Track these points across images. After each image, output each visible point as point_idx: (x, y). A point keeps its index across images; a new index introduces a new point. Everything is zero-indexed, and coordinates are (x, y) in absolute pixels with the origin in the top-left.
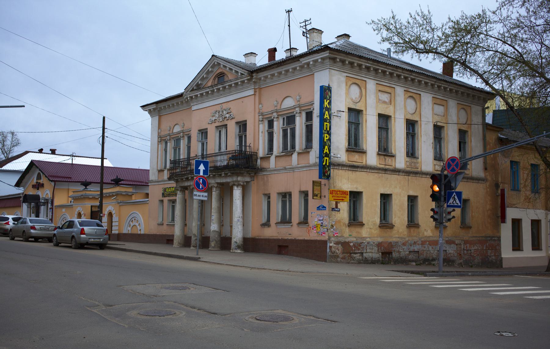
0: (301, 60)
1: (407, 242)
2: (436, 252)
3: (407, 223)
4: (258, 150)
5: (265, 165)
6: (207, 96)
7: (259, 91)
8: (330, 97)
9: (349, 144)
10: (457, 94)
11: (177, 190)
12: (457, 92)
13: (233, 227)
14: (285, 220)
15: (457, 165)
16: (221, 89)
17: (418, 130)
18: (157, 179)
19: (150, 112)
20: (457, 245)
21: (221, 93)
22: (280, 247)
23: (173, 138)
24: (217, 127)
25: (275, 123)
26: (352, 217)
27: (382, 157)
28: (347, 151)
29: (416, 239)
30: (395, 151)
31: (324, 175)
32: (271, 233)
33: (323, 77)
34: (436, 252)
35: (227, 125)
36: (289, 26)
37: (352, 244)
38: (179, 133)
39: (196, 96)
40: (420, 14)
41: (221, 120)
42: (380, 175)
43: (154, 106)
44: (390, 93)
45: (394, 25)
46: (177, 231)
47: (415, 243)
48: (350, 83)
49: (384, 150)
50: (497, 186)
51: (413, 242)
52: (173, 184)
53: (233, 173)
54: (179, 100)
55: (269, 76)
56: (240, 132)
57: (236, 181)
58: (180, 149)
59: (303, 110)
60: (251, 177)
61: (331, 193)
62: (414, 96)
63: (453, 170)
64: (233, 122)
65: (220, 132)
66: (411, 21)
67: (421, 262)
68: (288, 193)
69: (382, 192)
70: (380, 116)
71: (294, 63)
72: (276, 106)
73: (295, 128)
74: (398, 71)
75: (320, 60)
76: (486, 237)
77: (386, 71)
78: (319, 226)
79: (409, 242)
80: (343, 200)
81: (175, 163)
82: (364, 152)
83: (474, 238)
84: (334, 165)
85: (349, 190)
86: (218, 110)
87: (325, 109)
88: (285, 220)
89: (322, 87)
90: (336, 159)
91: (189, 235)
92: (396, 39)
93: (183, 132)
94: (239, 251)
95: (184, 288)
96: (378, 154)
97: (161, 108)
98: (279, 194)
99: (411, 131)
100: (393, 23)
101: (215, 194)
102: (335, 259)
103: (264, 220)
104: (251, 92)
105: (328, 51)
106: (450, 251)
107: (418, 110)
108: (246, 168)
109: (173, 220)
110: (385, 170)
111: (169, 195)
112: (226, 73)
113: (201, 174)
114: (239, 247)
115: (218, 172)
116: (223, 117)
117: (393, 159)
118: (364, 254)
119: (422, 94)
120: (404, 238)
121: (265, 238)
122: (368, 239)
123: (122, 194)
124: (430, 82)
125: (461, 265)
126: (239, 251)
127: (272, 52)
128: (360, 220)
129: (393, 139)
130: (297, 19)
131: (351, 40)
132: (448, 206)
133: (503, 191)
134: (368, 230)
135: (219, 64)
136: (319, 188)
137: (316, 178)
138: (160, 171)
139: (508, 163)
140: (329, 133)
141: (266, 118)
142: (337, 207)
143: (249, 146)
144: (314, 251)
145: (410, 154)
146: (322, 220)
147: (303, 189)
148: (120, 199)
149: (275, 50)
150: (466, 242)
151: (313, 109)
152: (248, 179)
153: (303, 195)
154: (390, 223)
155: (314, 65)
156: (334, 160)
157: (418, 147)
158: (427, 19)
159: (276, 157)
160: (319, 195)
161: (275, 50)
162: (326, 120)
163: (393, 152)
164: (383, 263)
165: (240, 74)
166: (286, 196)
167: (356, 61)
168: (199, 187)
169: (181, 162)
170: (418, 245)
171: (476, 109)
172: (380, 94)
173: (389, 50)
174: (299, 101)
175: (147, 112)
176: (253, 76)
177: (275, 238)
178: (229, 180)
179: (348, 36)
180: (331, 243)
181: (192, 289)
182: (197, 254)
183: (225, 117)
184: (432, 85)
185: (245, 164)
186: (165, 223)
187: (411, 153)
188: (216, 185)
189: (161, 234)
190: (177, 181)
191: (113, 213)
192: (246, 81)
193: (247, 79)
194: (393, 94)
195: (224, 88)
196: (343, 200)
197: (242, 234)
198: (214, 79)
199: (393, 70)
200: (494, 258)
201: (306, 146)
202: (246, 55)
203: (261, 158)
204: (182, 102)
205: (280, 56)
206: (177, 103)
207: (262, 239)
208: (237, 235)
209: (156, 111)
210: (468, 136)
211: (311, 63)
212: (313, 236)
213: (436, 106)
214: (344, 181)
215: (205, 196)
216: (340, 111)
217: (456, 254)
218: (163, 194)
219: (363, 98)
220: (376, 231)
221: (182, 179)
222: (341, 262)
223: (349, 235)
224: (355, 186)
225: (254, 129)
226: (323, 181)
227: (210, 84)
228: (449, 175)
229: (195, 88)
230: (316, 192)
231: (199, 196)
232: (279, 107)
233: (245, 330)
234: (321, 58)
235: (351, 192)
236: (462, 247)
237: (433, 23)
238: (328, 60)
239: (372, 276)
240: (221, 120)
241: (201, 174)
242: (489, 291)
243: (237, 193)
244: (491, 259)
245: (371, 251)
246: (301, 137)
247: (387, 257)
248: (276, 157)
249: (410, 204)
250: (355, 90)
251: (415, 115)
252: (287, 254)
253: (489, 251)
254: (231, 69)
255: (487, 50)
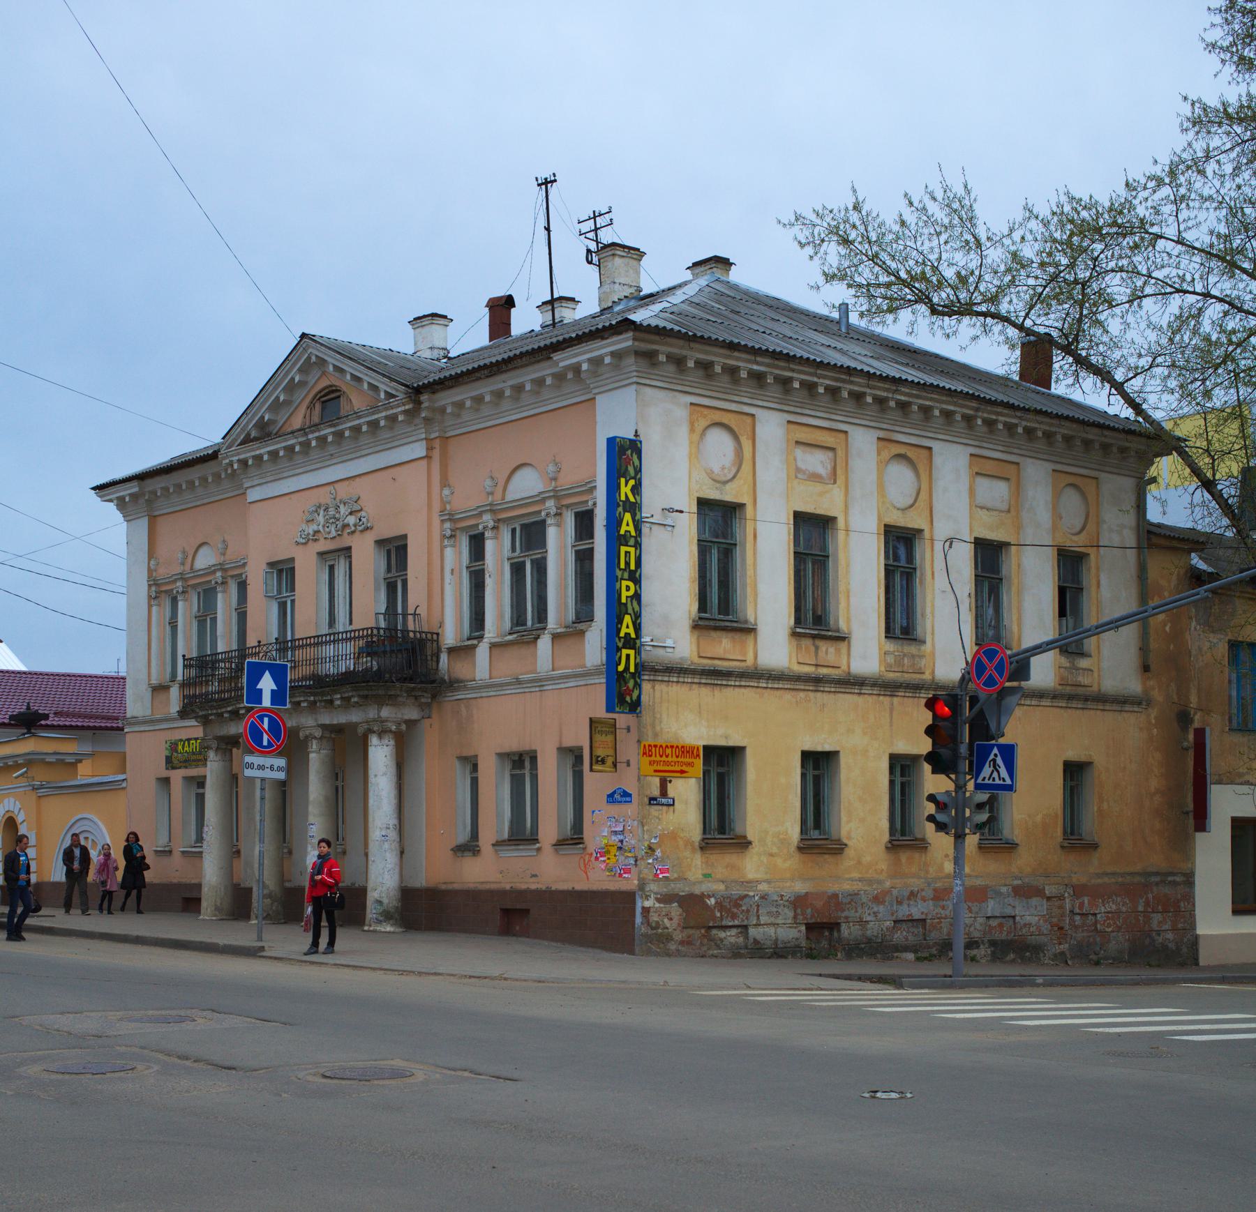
0: (556, 356)
1: (889, 892)
2: (980, 920)
3: (886, 837)
4: (441, 625)
5: (461, 669)
6: (291, 459)
7: (440, 447)
8: (638, 470)
9: (703, 606)
10: (1050, 444)
11: (209, 748)
12: (1048, 436)
13: (371, 858)
14: (522, 835)
15: (1000, 668)
16: (330, 439)
17: (923, 559)
18: (148, 712)
19: (121, 505)
20: (1049, 899)
21: (332, 449)
22: (507, 912)
23: (194, 587)
24: (321, 554)
25: (489, 546)
26: (714, 822)
27: (807, 642)
28: (696, 627)
29: (915, 883)
30: (848, 620)
31: (622, 701)
32: (486, 871)
33: (617, 413)
34: (980, 920)
35: (349, 548)
36: (548, 229)
37: (713, 901)
38: (210, 571)
39: (259, 458)
40: (939, 195)
41: (334, 533)
42: (802, 694)
43: (134, 488)
44: (833, 449)
45: (862, 228)
46: (211, 873)
47: (913, 895)
48: (702, 423)
49: (814, 618)
50: (1184, 718)
51: (906, 894)
52: (193, 729)
53: (366, 697)
54: (208, 469)
55: (468, 403)
56: (389, 570)
57: (374, 720)
58: (214, 620)
59: (568, 506)
60: (422, 707)
61: (648, 751)
62: (911, 453)
63: (990, 682)
64: (370, 538)
65: (332, 568)
66: (911, 218)
67: (934, 951)
68: (527, 753)
69: (806, 748)
70: (802, 520)
71: (536, 366)
72: (492, 493)
73: (545, 559)
74: (852, 383)
75: (607, 360)
76: (1147, 874)
77: (815, 385)
78: (614, 850)
79: (895, 892)
80: (682, 772)
81: (203, 665)
82: (748, 630)
83: (1106, 880)
84: (654, 670)
85: (702, 743)
86: (323, 501)
87: (625, 508)
88: (522, 835)
89: (611, 441)
90: (661, 652)
91: (247, 885)
92: (866, 273)
93: (221, 567)
94: (389, 929)
95: (181, 1020)
96: (794, 634)
97: (154, 493)
98: (502, 756)
99: (903, 563)
100: (858, 223)
101: (316, 759)
102: (658, 944)
103: (463, 836)
104: (419, 450)
105: (630, 334)
106: (1028, 919)
107: (923, 496)
108: (404, 680)
109: (200, 839)
110: (817, 682)
111: (186, 763)
112: (344, 388)
113: (266, 702)
114: (387, 916)
115: (323, 694)
116: (340, 524)
117: (843, 645)
118: (752, 932)
119: (936, 446)
120: (879, 882)
121: (466, 887)
122: (763, 887)
123: (43, 762)
124: (959, 411)
125: (1061, 959)
126: (389, 929)
127: (501, 308)
128: (738, 830)
129: (842, 588)
130: (571, 205)
131: (735, 276)
132: (978, 787)
133: (1200, 733)
134: (764, 859)
135: (322, 362)
136: (610, 738)
137: (600, 712)
138: (159, 689)
139: (1223, 649)
140: (635, 578)
141: (462, 529)
142: (664, 793)
143: (415, 614)
144: (597, 921)
145: (898, 632)
146: (622, 832)
147: (569, 742)
148: (40, 775)
149: (509, 302)
150: (1079, 890)
151: (595, 504)
152: (412, 713)
153: (570, 761)
154: (834, 837)
155: (595, 374)
156: (649, 654)
157: (924, 609)
158: (962, 213)
159: (493, 646)
160: (610, 761)
161: (509, 302)
162: (624, 540)
163: (842, 625)
164: (811, 955)
165: (382, 395)
166: (521, 763)
167: (720, 360)
168: (260, 743)
169: (222, 661)
170: (924, 899)
171: (1117, 485)
172: (799, 452)
173: (844, 309)
174: (555, 479)
175: (112, 507)
176: (420, 403)
177: (493, 886)
178: (355, 716)
179: (723, 263)
180: (647, 898)
181: (200, 1021)
182: (260, 939)
183: (346, 526)
184: (968, 419)
185: (404, 668)
186: (178, 849)
187: (901, 623)
188: (318, 733)
189: (164, 881)
190: (205, 721)
191: (19, 819)
192: (401, 418)
193: (405, 412)
194: (840, 453)
195: (339, 435)
196: (682, 772)
197: (396, 877)
198: (311, 407)
199: (836, 380)
200: (1170, 936)
201: (577, 613)
202: (418, 321)
203: (451, 650)
204: (217, 476)
205: (525, 320)
206: (204, 480)
207: (456, 893)
208: (382, 878)
209: (142, 501)
210: (1089, 570)
211: (585, 367)
212: (598, 878)
213: (983, 483)
214: (687, 718)
215: (279, 769)
216: (671, 510)
217: (1046, 928)
218: (169, 761)
219: (747, 467)
220: (789, 863)
221: (221, 715)
222: (678, 954)
223: (701, 873)
224: (720, 731)
225: (429, 564)
226: (623, 719)
227: (297, 422)
228: (982, 696)
229: (253, 434)
230: (600, 752)
231: (261, 767)
232: (498, 496)
233: (284, 1095)
234: (613, 354)
235: (709, 750)
236: (1068, 906)
237: (980, 223)
238: (631, 360)
239: (728, 989)
240: (334, 533)
241: (266, 702)
242: (933, 1012)
243: (380, 755)
244: (1160, 939)
245: (772, 920)
246: (562, 587)
247: (825, 936)
248: (493, 646)
249: (898, 780)
250: (719, 446)
251: (912, 512)
252: (525, 933)
253: (1156, 918)
254: (358, 380)
255: (1178, 291)
